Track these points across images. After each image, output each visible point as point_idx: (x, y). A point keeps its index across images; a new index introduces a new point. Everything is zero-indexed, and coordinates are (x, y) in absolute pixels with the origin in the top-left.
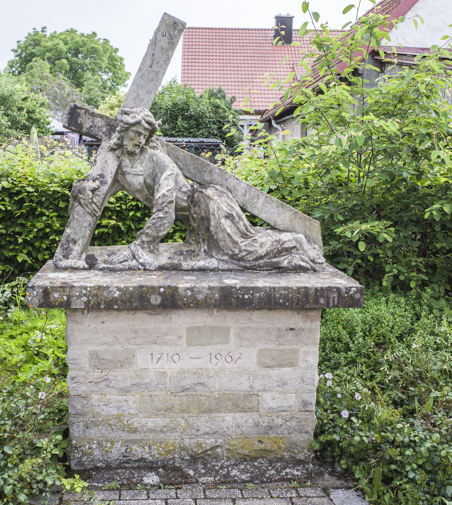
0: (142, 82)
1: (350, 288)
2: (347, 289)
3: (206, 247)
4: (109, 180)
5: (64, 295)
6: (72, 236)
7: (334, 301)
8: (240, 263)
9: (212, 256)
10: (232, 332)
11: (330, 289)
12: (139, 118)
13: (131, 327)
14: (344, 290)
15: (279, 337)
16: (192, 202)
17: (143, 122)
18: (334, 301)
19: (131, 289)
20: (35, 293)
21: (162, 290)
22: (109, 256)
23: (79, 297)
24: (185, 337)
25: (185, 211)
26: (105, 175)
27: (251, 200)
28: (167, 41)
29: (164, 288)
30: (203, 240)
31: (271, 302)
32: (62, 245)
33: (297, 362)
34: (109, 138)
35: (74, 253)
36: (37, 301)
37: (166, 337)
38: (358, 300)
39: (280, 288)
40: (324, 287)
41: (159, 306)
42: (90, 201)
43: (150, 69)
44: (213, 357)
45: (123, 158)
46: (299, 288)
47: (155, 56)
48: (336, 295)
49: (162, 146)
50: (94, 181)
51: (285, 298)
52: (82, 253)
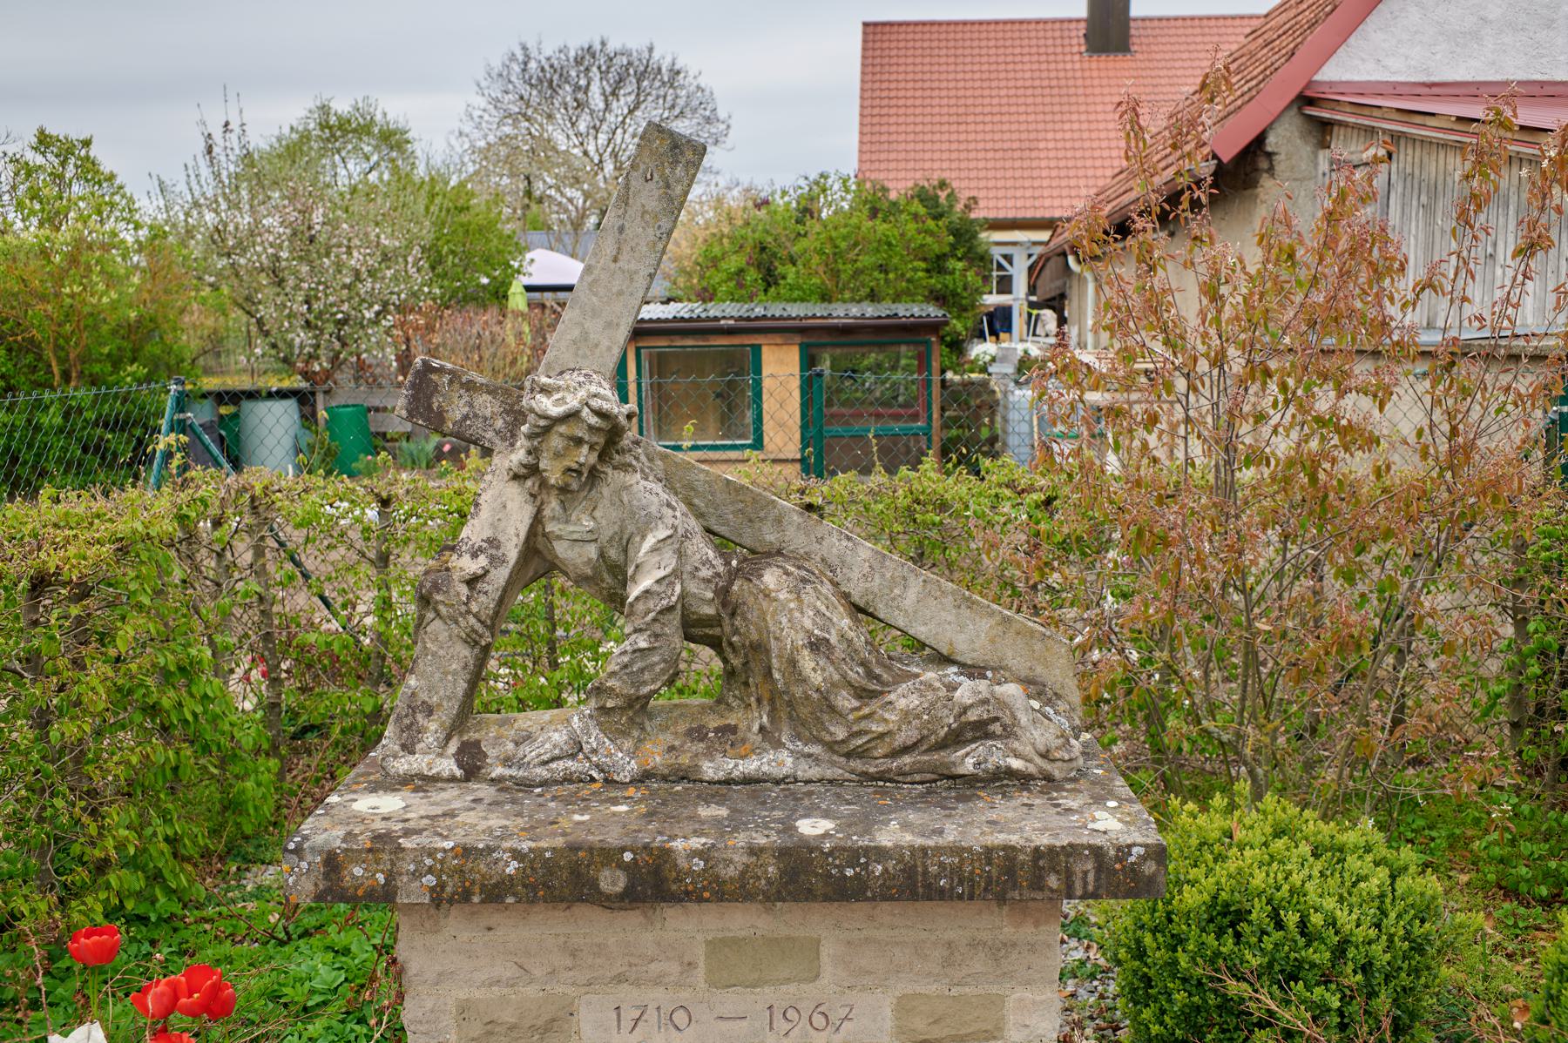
0: (594, 299)
1: (1130, 846)
2: (1119, 849)
3: (765, 719)
4: (512, 554)
5: (377, 871)
6: (423, 696)
7: (1085, 884)
8: (852, 764)
9: (778, 745)
10: (827, 951)
11: (1072, 850)
12: (573, 402)
13: (562, 939)
14: (1112, 853)
15: (947, 963)
16: (724, 604)
17: (585, 412)
18: (1084, 879)
19: (548, 855)
20: (304, 865)
21: (628, 856)
22: (517, 744)
23: (416, 875)
24: (702, 964)
25: (712, 626)
26: (502, 539)
27: (886, 591)
28: (657, 193)
29: (632, 851)
30: (759, 701)
31: (915, 886)
32: (399, 719)
33: (1000, 1029)
34: (512, 445)
35: (430, 739)
36: (309, 887)
37: (653, 966)
38: (1151, 880)
39: (938, 850)
40: (1058, 844)
41: (622, 897)
42: (463, 608)
43: (613, 265)
44: (778, 1015)
45: (545, 496)
46: (989, 851)
47: (627, 231)
48: (1090, 866)
49: (651, 460)
50: (474, 556)
51: (956, 873)
52: (448, 738)
